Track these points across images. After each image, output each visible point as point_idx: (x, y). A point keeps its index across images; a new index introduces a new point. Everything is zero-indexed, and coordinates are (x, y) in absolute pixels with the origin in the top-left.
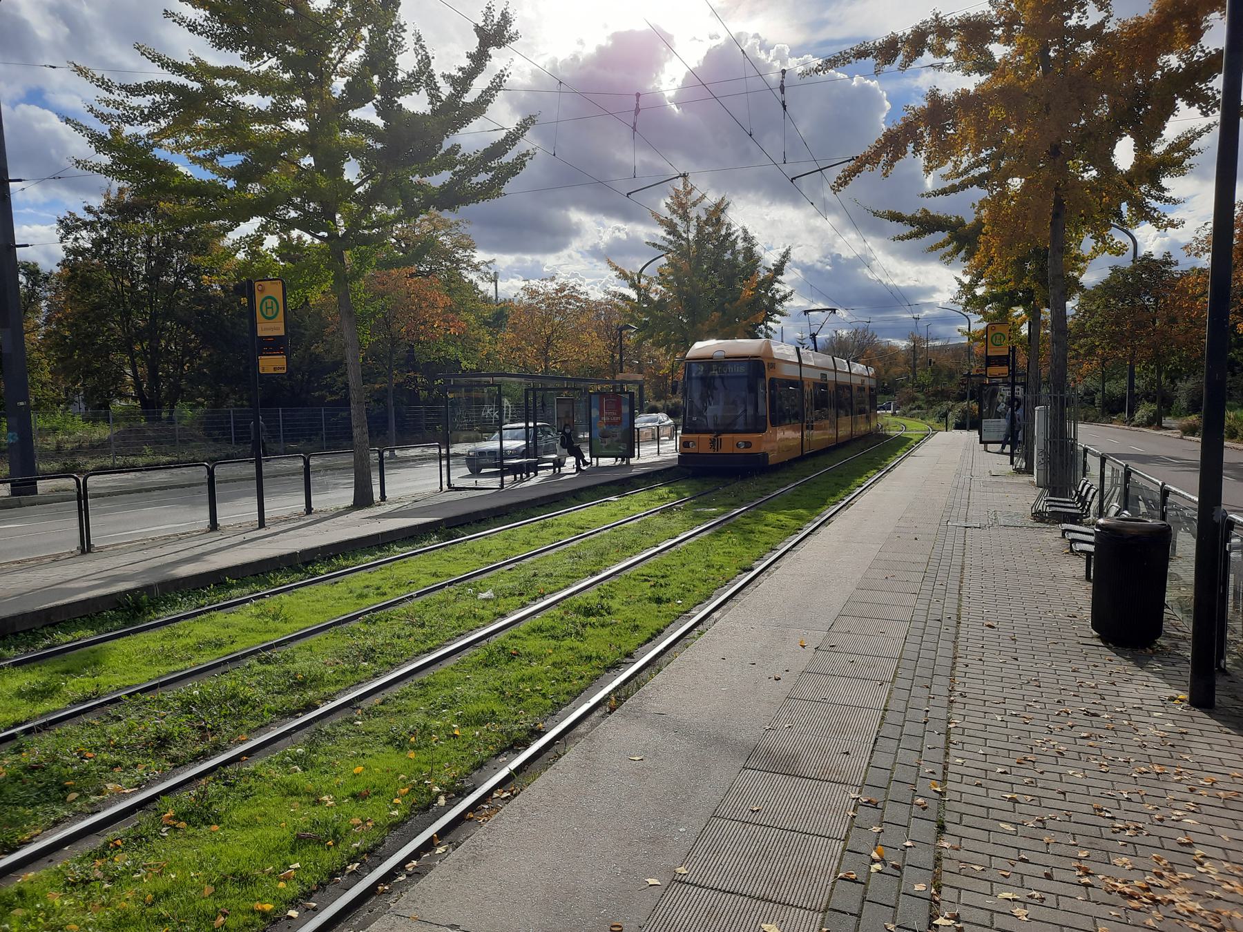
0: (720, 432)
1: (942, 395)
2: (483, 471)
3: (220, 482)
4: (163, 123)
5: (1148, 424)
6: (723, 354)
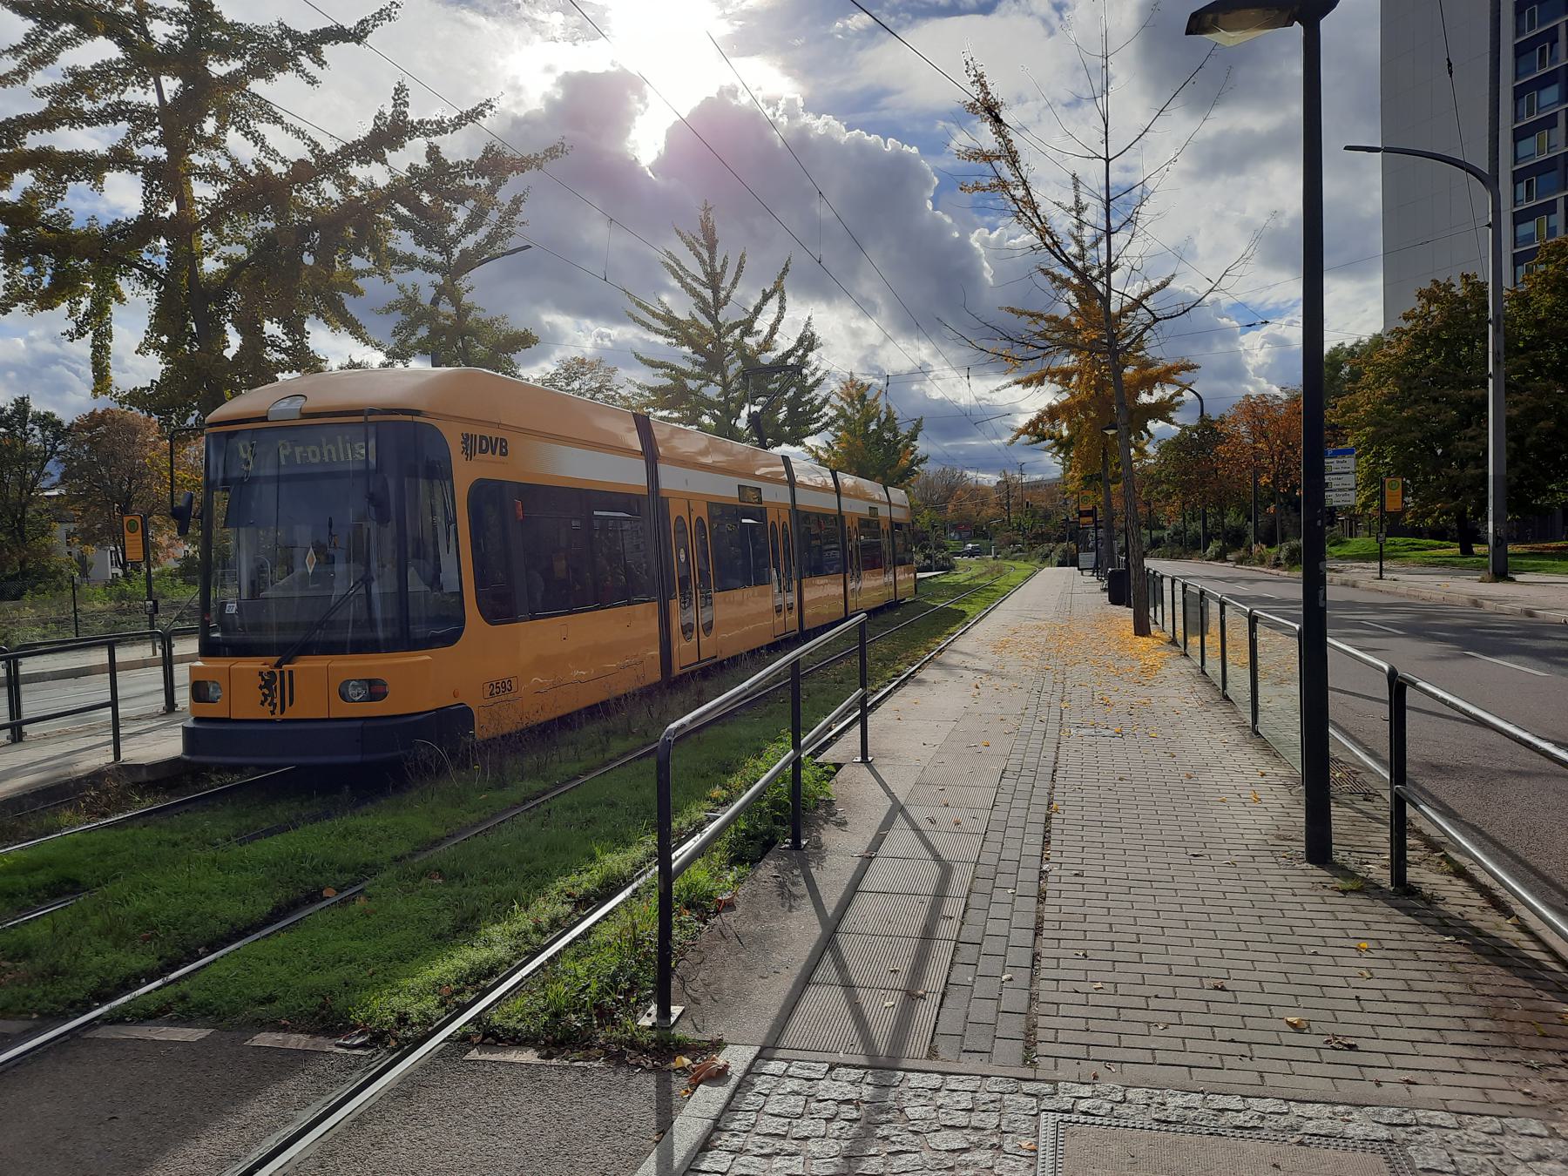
0: (288, 652)
1: (1043, 538)
5: (1216, 559)
6: (298, 404)
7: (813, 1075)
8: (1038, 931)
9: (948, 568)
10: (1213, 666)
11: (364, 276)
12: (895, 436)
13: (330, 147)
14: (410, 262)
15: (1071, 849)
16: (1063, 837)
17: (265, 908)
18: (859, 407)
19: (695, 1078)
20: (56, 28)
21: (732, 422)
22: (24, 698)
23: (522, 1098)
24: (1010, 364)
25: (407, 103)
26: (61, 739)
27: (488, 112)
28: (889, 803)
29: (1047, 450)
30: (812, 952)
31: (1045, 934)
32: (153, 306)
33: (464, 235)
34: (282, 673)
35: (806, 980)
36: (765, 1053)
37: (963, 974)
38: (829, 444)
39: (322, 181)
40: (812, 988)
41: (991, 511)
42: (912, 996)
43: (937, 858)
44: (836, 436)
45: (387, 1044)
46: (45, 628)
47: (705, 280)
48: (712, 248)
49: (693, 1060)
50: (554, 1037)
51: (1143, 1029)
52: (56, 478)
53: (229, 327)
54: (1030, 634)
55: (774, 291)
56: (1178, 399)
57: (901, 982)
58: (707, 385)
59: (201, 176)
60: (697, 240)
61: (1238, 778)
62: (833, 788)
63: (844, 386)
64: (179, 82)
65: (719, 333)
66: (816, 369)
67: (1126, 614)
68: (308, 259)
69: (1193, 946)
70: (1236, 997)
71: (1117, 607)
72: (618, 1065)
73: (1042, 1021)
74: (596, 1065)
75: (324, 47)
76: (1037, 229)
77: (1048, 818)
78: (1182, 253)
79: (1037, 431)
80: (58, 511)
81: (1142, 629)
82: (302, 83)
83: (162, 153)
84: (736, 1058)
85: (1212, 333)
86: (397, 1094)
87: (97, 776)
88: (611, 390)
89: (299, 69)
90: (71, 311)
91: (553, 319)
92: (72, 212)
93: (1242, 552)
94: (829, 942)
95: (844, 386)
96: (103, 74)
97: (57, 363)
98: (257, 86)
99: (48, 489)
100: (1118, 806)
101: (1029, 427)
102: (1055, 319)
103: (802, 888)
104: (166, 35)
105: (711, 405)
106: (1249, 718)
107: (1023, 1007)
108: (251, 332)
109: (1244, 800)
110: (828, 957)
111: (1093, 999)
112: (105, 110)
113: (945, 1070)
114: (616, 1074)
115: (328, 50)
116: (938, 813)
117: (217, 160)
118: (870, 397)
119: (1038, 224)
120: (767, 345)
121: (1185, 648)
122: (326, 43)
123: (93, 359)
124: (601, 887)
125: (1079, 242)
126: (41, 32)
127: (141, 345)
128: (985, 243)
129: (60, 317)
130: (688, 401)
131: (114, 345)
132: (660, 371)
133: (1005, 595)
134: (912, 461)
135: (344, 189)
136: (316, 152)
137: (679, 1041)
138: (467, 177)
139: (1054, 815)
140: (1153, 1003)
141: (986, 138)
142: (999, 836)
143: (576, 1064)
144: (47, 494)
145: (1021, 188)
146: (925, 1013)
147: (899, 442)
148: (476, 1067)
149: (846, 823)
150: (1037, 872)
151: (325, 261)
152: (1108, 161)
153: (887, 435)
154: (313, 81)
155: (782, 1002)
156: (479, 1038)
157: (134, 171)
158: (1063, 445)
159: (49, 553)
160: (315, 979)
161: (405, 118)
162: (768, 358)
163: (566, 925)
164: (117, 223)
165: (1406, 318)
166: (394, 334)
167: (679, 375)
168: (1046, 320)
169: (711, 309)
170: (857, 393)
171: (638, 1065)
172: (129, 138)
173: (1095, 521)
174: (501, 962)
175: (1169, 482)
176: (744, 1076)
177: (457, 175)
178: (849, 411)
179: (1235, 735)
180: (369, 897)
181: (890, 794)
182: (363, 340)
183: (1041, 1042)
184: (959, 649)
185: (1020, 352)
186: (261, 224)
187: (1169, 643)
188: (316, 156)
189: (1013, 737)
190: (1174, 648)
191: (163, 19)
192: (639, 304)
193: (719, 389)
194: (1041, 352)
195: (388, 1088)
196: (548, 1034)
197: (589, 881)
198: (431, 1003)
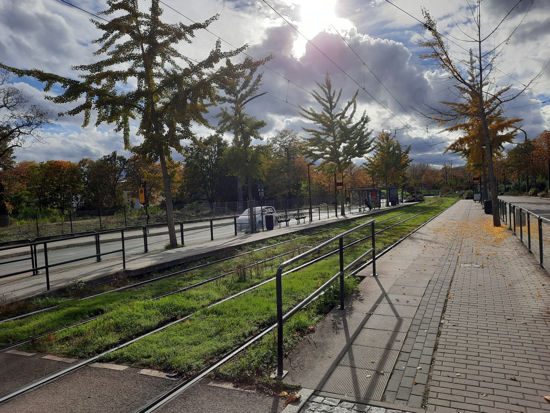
1: (460, 189)
2: (242, 230)
3: (180, 237)
4: (366, 142)
7: (333, 404)
8: (435, 349)
9: (422, 201)
10: (525, 239)
11: (208, 106)
12: (400, 152)
13: (195, 64)
14: (224, 100)
15: (454, 314)
16: (452, 309)
17: (156, 323)
18: (386, 142)
19: (288, 401)
20: (112, 32)
21: (337, 149)
22: (101, 248)
23: (223, 403)
24: (441, 122)
25: (220, 46)
26: (112, 261)
27: (246, 48)
28: (381, 292)
29: (461, 155)
30: (341, 352)
31: (438, 350)
32: (141, 120)
33: (242, 89)
35: (337, 363)
36: (316, 393)
37: (401, 366)
38: (375, 156)
39: (193, 75)
40: (339, 367)
41: (439, 179)
42: (378, 373)
43: (397, 316)
44: (377, 153)
45: (183, 377)
46: (117, 224)
47: (327, 99)
48: (329, 87)
49: (288, 393)
50: (240, 379)
51: (476, 395)
52: (124, 177)
53: (165, 125)
54: (450, 226)
55: (352, 102)
56: (514, 133)
57: (374, 367)
58: (327, 137)
59: (155, 76)
60: (324, 86)
61: (532, 287)
62: (360, 286)
63: (380, 135)
64: (147, 45)
65: (332, 118)
66: (367, 129)
67: (491, 217)
68: (189, 101)
69: (503, 359)
70: (521, 384)
71: (488, 215)
72: (261, 392)
73: (432, 388)
74: (253, 392)
75: (194, 30)
76: (451, 70)
77: (446, 301)
78: (513, 77)
79: (456, 147)
80: (125, 187)
81: (497, 223)
82: (187, 42)
83: (143, 69)
84: (304, 394)
85: (528, 106)
86: (182, 397)
87: (117, 274)
88: (296, 140)
89: (186, 39)
90: (117, 123)
91: (270, 116)
92: (116, 91)
93: (544, 193)
94: (348, 349)
95: (380, 135)
96: (127, 46)
97: (116, 140)
98: (172, 45)
99: (122, 180)
100: (477, 297)
101: (452, 146)
102: (462, 105)
103: (342, 326)
104: (144, 30)
105: (329, 144)
106: (539, 260)
107: (424, 382)
108: (173, 128)
109: (533, 296)
110: (347, 355)
111: (456, 380)
112: (126, 57)
113: (387, 407)
114: (259, 396)
115: (195, 31)
116: (400, 297)
117: (160, 70)
118: (390, 138)
119: (451, 68)
120: (349, 122)
121: (515, 231)
122: (194, 29)
123: (124, 137)
124: (269, 320)
125: (472, 75)
126: (108, 33)
127: (138, 132)
128: (430, 77)
129: (114, 125)
130: (321, 143)
131: (130, 133)
132: (311, 133)
133: (443, 211)
134: (407, 161)
135: (200, 77)
136: (191, 65)
137: (284, 385)
138: (239, 69)
139: (448, 300)
140: (482, 384)
141: (428, 35)
142: (424, 308)
143: (246, 391)
144: (122, 182)
145: (444, 55)
146: (383, 380)
147: (402, 154)
148: (211, 389)
149: (363, 300)
150: (438, 323)
151: (194, 101)
152: (480, 42)
153: (397, 152)
154: (190, 42)
155: (326, 372)
156: (214, 377)
157: (135, 76)
158: (466, 153)
159: (122, 200)
160: (165, 350)
161: (220, 51)
162: (350, 126)
163: (255, 334)
164: (130, 93)
166: (219, 125)
167: (318, 134)
168: (458, 105)
169: (329, 110)
170: (386, 137)
171: (268, 393)
172: (134, 65)
173: (480, 182)
174: (229, 348)
175: (512, 166)
176: (306, 402)
177: (236, 69)
178: (382, 144)
179: (533, 268)
180: (190, 320)
181: (382, 289)
182: (208, 126)
183: (430, 397)
184: (420, 232)
185: (444, 118)
186: (174, 90)
187: (508, 229)
188: (191, 67)
189: (436, 267)
190: (510, 231)
191: (143, 25)
192: (304, 110)
193: (332, 138)
194: (454, 117)
195: (179, 394)
196: (238, 378)
197: (266, 318)
198: (200, 362)
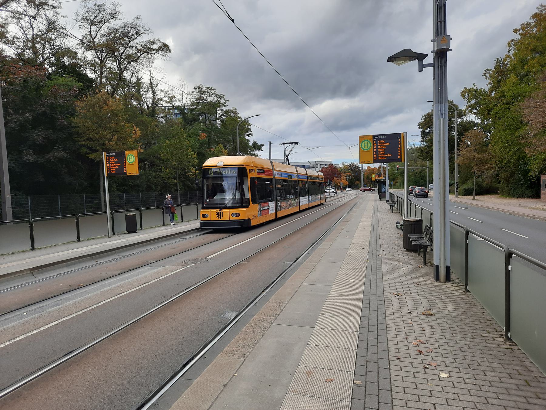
6: (222, 164)
34: (220, 212)
59: (422, 252)
165: (517, 39)
